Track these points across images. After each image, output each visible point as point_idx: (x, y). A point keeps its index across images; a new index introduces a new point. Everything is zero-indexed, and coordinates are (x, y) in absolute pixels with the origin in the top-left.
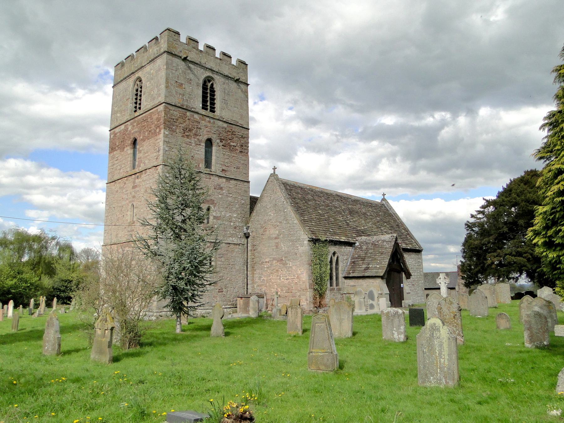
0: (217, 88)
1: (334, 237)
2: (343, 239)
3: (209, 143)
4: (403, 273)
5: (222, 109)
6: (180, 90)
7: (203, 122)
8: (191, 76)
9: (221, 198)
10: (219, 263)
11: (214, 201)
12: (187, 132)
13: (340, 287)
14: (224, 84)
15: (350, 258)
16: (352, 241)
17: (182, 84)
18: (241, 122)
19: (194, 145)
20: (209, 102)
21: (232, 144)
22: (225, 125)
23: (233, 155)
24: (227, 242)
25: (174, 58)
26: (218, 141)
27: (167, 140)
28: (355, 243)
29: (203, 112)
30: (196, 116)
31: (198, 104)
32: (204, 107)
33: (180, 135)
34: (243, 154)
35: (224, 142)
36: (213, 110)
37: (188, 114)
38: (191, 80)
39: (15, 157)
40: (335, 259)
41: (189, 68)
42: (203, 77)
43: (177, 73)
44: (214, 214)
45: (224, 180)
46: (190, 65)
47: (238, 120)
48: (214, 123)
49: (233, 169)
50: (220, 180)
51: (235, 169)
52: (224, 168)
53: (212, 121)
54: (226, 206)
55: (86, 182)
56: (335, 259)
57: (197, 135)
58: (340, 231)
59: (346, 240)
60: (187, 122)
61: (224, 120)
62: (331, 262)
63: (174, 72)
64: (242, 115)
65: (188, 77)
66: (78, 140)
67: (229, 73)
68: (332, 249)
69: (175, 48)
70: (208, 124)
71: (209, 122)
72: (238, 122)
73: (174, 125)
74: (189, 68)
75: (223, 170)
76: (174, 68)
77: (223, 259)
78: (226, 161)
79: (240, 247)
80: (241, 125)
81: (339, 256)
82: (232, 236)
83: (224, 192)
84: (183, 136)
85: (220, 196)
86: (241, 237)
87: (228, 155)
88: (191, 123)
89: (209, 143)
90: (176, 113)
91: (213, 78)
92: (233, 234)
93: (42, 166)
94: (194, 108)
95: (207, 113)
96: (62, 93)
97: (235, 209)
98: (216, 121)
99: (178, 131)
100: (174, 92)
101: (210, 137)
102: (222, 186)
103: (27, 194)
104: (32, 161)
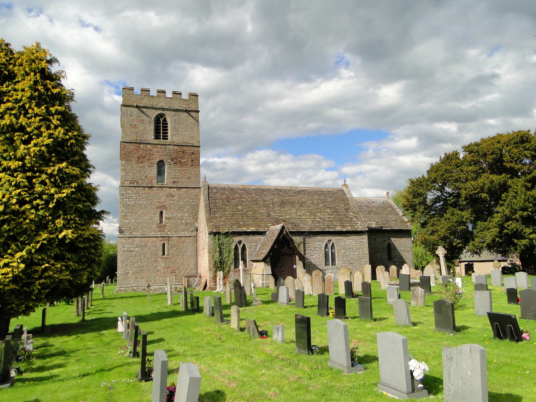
0: (169, 120)
1: (240, 229)
2: (252, 229)
3: (161, 164)
4: (297, 256)
5: (172, 136)
6: (133, 130)
7: (155, 149)
8: (145, 117)
9: (172, 203)
10: (172, 251)
11: (166, 206)
12: (140, 159)
13: (248, 268)
14: (175, 116)
15: (260, 245)
16: (261, 230)
17: (135, 125)
18: (191, 142)
19: (147, 167)
20: (162, 133)
21: (183, 160)
22: (176, 148)
23: (184, 169)
24: (178, 235)
25: (128, 108)
26: (170, 161)
27: (124, 168)
28: (265, 232)
29: (156, 142)
30: (149, 146)
31: (150, 136)
32: (157, 137)
33: (135, 162)
34: (193, 167)
35: (175, 160)
36: (165, 138)
37: (141, 146)
38: (143, 120)
39: (260, 149)
40: (240, 247)
41: (142, 112)
42: (155, 115)
43: (132, 118)
44: (166, 216)
45: (175, 189)
46: (142, 109)
47: (188, 141)
48: (166, 148)
49: (183, 180)
50: (172, 190)
51: (187, 180)
52: (175, 180)
53: (163, 147)
54: (177, 209)
55: (312, 163)
56: (240, 247)
57: (150, 160)
58: (254, 223)
59: (255, 230)
60: (141, 152)
61: (175, 144)
62: (236, 248)
63: (128, 118)
64: (193, 136)
65: (141, 119)
66: (312, 126)
67: (179, 107)
68: (237, 239)
69: (130, 100)
70: (160, 150)
71: (161, 148)
72: (188, 143)
73: (129, 157)
74: (142, 112)
75: (174, 182)
76: (129, 115)
77: (175, 249)
78: (177, 174)
79: (191, 238)
80: (192, 144)
81: (245, 244)
82: (184, 230)
83: (175, 198)
84: (137, 163)
85: (171, 202)
86: (192, 231)
87: (179, 169)
88: (144, 152)
89: (161, 164)
90: (132, 147)
91: (164, 114)
92: (185, 229)
93: (280, 153)
94: (147, 140)
95: (161, 141)
96: (303, 86)
97: (185, 210)
98: (167, 146)
99: (133, 160)
100: (129, 132)
101: (161, 159)
102: (173, 194)
103: (266, 179)
104: (273, 150)
